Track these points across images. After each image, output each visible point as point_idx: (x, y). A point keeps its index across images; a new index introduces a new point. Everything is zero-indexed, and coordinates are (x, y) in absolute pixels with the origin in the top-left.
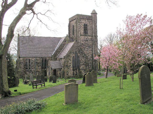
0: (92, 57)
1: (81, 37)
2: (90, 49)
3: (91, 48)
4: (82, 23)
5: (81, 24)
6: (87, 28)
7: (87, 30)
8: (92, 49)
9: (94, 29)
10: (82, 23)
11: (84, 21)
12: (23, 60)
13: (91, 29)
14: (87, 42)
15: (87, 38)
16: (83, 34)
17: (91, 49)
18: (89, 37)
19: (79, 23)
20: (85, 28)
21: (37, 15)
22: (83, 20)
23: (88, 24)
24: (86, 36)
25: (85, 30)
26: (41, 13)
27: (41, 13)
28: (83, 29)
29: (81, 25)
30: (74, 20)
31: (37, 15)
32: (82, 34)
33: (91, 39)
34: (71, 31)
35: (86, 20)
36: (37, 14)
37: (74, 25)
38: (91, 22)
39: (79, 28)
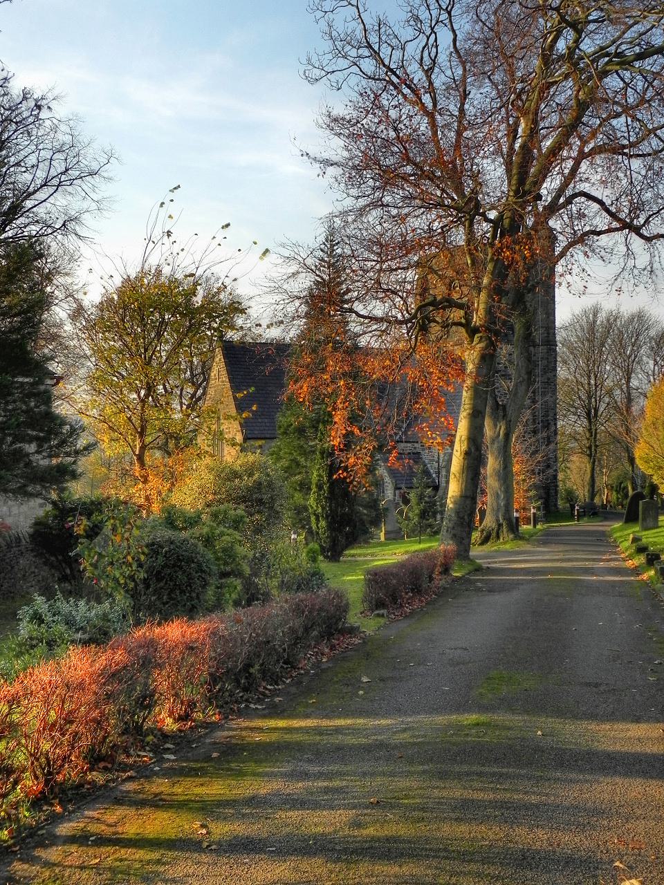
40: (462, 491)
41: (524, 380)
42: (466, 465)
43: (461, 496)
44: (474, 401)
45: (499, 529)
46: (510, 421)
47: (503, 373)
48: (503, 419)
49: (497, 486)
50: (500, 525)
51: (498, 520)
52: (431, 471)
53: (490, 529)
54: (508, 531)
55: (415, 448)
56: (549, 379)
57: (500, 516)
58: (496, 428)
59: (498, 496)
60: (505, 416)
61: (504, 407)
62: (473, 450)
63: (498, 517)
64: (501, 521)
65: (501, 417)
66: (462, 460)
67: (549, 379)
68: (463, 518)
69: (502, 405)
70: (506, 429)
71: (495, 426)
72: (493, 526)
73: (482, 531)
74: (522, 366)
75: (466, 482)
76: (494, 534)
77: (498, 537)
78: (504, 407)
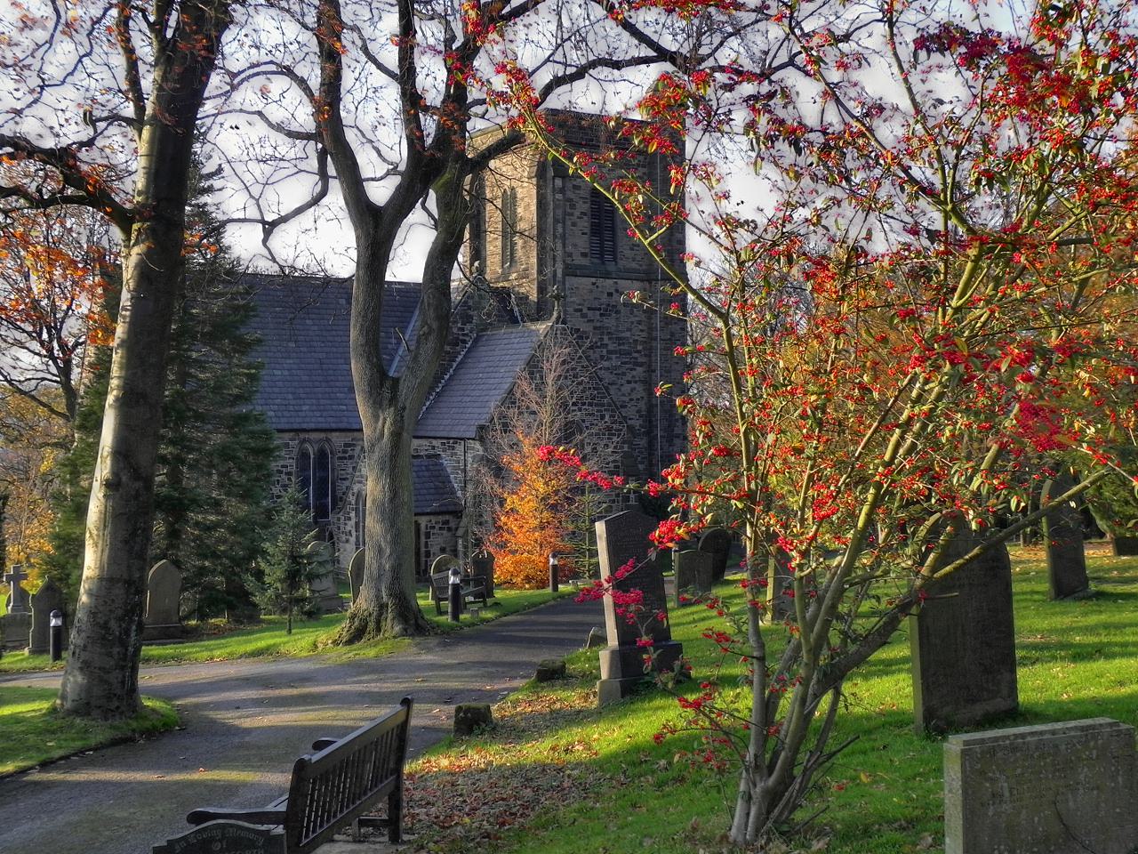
40: (101, 568)
41: (431, 330)
42: (110, 508)
43: (101, 579)
44: (127, 370)
45: (380, 615)
46: (404, 409)
47: (598, 324)
48: (390, 406)
49: (379, 532)
50: (382, 607)
51: (378, 597)
52: (456, 485)
53: (366, 613)
54: (394, 618)
55: (433, 448)
56: (672, 334)
57: (383, 589)
58: (377, 421)
59: (380, 551)
60: (393, 400)
61: (396, 381)
62: (124, 479)
63: (379, 590)
64: (385, 599)
65: (386, 402)
66: (103, 500)
67: (672, 334)
68: (105, 626)
69: (393, 379)
70: (394, 423)
71: (376, 417)
72: (371, 609)
73: (353, 617)
74: (429, 304)
75: (111, 549)
76: (371, 625)
77: (378, 629)
78: (396, 381)
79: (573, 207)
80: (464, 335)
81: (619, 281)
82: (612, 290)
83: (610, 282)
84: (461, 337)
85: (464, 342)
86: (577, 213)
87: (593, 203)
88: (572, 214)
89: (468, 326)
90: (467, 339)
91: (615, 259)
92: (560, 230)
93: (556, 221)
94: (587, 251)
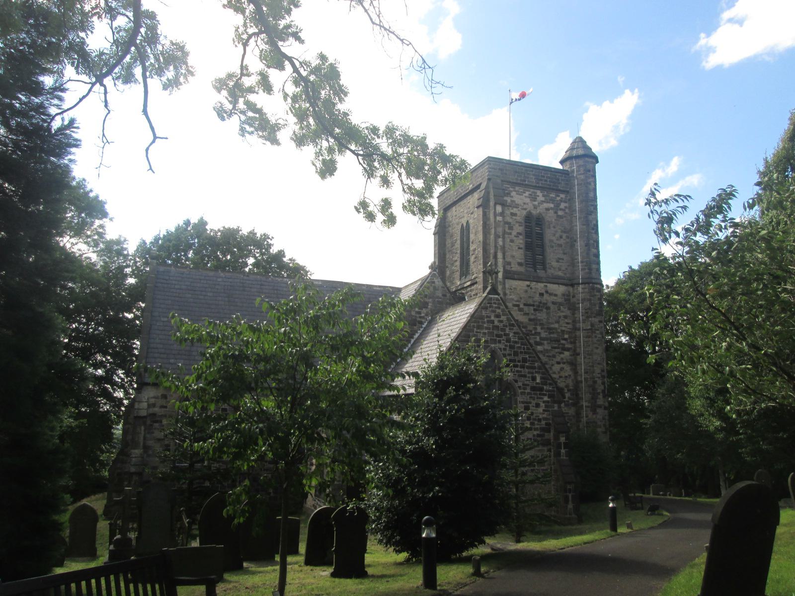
0: (574, 405)
1: (511, 283)
2: (558, 359)
3: (568, 350)
4: (515, 210)
5: (508, 212)
6: (541, 236)
7: (542, 246)
8: (576, 354)
9: (579, 245)
10: (515, 210)
11: (528, 200)
12: (163, 402)
13: (562, 242)
14: (542, 316)
15: (546, 296)
16: (522, 269)
17: (567, 353)
18: (552, 287)
19: (499, 209)
20: (528, 234)
21: (154, 142)
22: (519, 193)
23: (550, 217)
24: (538, 280)
25: (529, 247)
26: (108, 114)
27: (108, 114)
28: (520, 241)
29: (508, 219)
30: (472, 192)
31: (154, 142)
32: (515, 268)
33: (567, 297)
34: (456, 257)
35: (539, 193)
36: (155, 137)
37: (471, 221)
38: (563, 205)
39: (500, 230)
79: (511, 228)
80: (420, 317)
81: (548, 285)
82: (543, 291)
83: (542, 285)
84: (419, 319)
85: (421, 323)
86: (514, 233)
87: (526, 227)
88: (510, 234)
89: (424, 310)
90: (423, 320)
91: (544, 269)
92: (501, 243)
93: (497, 236)
94: (523, 261)
